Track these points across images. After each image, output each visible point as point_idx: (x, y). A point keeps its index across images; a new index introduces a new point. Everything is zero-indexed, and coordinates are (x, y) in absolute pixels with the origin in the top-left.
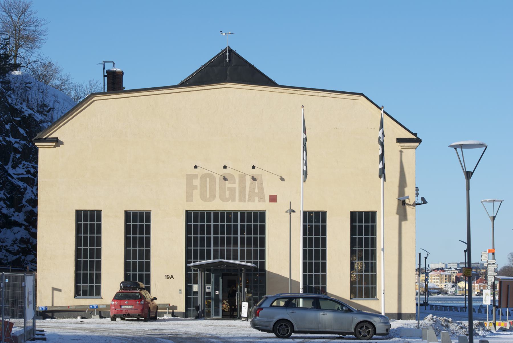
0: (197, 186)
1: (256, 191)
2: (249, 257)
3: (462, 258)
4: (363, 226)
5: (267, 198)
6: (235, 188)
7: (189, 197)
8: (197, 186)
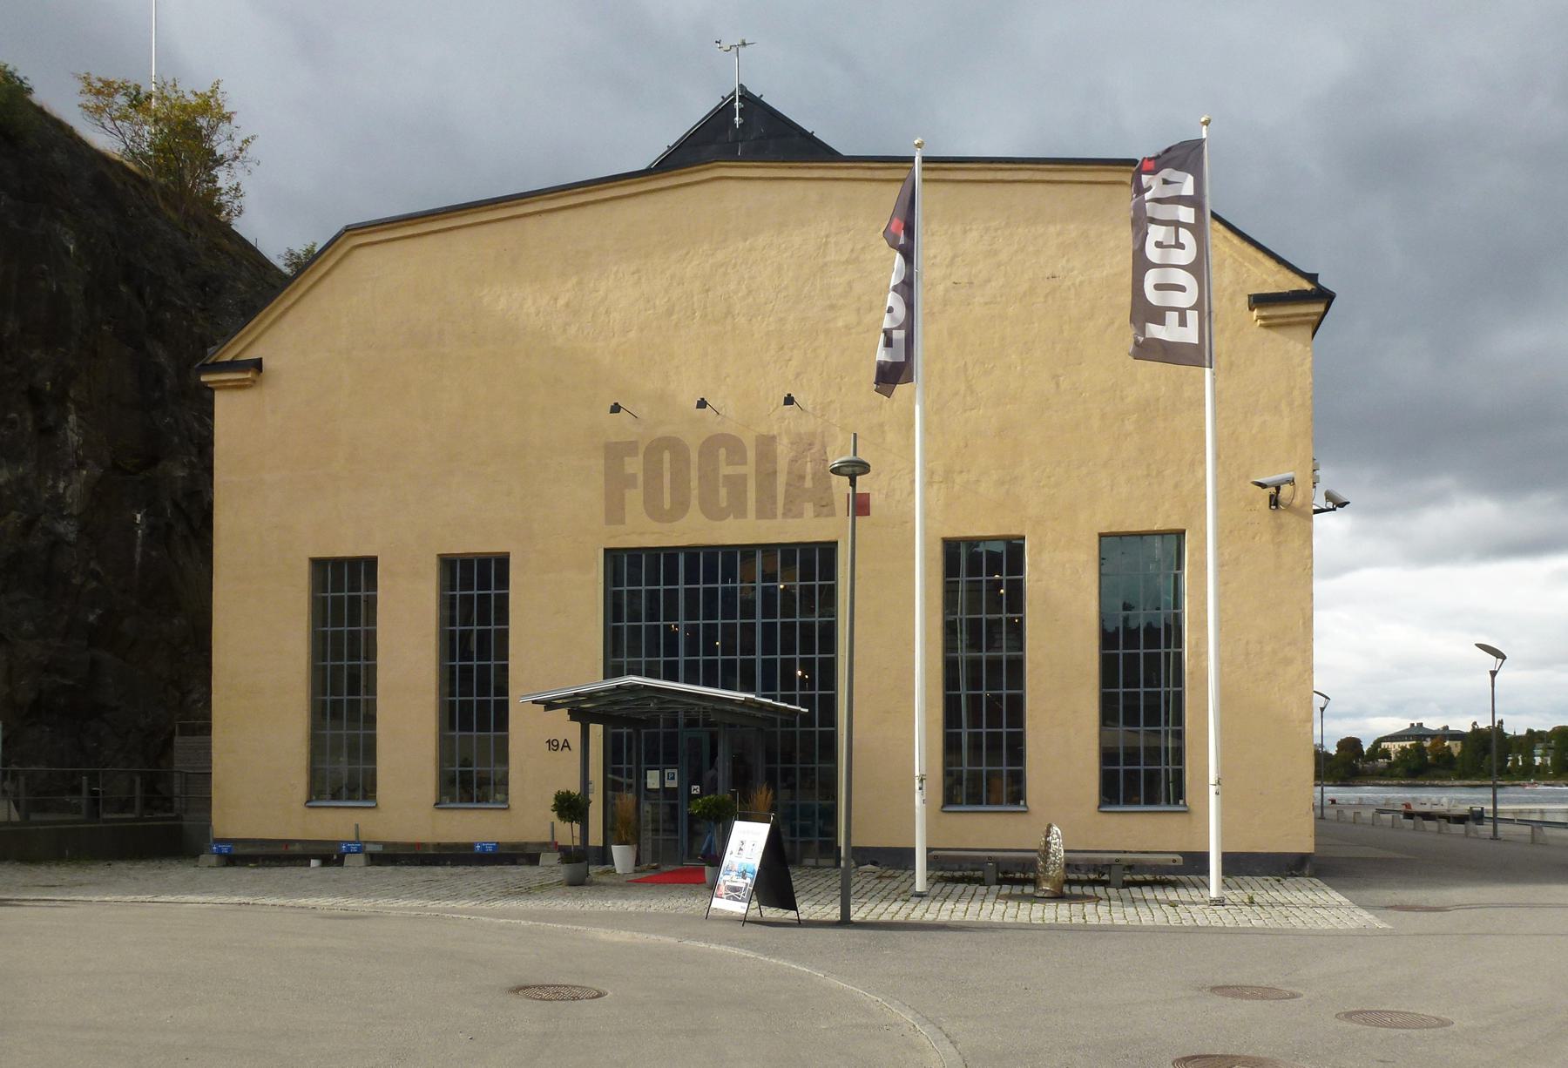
0: (634, 476)
6: (744, 478)
7: (615, 512)
8: (634, 476)
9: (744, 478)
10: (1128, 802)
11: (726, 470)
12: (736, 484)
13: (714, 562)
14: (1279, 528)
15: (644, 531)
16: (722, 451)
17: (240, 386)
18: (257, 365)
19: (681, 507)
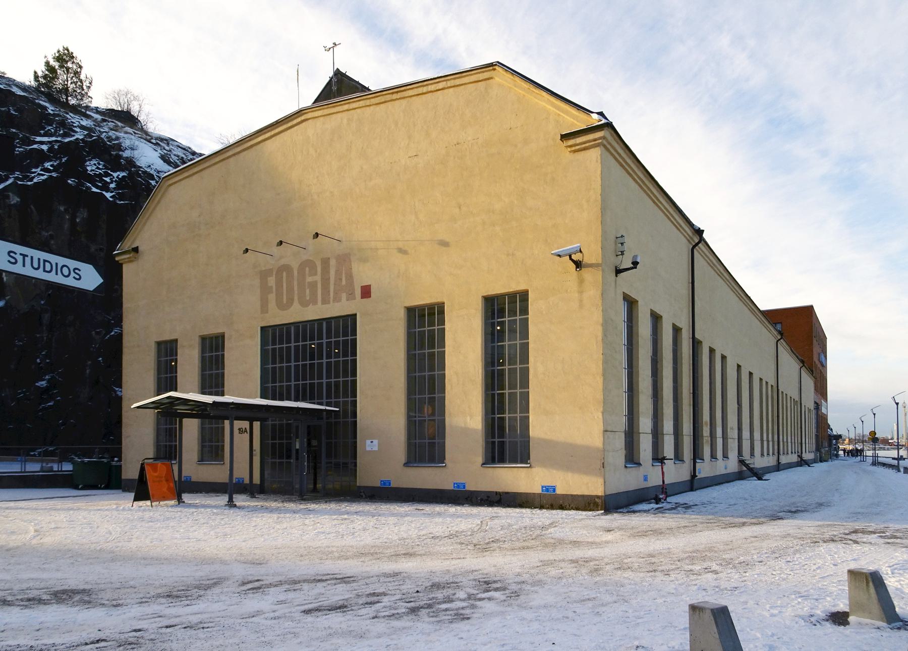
0: (272, 287)
1: (344, 282)
2: (320, 397)
3: (665, 467)
4: (504, 316)
5: (358, 292)
6: (316, 282)
7: (264, 308)
8: (272, 287)
9: (316, 282)
10: (511, 462)
11: (309, 279)
12: (313, 285)
13: (444, 313)
14: (581, 281)
15: (279, 317)
16: (307, 269)
17: (130, 261)
18: (136, 250)
19: (290, 301)
